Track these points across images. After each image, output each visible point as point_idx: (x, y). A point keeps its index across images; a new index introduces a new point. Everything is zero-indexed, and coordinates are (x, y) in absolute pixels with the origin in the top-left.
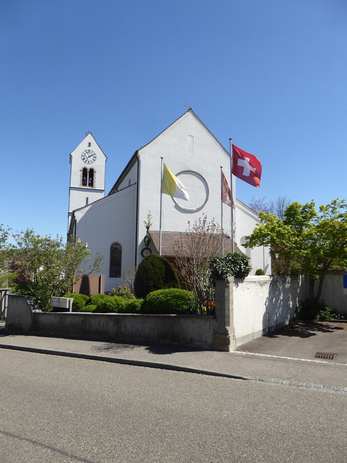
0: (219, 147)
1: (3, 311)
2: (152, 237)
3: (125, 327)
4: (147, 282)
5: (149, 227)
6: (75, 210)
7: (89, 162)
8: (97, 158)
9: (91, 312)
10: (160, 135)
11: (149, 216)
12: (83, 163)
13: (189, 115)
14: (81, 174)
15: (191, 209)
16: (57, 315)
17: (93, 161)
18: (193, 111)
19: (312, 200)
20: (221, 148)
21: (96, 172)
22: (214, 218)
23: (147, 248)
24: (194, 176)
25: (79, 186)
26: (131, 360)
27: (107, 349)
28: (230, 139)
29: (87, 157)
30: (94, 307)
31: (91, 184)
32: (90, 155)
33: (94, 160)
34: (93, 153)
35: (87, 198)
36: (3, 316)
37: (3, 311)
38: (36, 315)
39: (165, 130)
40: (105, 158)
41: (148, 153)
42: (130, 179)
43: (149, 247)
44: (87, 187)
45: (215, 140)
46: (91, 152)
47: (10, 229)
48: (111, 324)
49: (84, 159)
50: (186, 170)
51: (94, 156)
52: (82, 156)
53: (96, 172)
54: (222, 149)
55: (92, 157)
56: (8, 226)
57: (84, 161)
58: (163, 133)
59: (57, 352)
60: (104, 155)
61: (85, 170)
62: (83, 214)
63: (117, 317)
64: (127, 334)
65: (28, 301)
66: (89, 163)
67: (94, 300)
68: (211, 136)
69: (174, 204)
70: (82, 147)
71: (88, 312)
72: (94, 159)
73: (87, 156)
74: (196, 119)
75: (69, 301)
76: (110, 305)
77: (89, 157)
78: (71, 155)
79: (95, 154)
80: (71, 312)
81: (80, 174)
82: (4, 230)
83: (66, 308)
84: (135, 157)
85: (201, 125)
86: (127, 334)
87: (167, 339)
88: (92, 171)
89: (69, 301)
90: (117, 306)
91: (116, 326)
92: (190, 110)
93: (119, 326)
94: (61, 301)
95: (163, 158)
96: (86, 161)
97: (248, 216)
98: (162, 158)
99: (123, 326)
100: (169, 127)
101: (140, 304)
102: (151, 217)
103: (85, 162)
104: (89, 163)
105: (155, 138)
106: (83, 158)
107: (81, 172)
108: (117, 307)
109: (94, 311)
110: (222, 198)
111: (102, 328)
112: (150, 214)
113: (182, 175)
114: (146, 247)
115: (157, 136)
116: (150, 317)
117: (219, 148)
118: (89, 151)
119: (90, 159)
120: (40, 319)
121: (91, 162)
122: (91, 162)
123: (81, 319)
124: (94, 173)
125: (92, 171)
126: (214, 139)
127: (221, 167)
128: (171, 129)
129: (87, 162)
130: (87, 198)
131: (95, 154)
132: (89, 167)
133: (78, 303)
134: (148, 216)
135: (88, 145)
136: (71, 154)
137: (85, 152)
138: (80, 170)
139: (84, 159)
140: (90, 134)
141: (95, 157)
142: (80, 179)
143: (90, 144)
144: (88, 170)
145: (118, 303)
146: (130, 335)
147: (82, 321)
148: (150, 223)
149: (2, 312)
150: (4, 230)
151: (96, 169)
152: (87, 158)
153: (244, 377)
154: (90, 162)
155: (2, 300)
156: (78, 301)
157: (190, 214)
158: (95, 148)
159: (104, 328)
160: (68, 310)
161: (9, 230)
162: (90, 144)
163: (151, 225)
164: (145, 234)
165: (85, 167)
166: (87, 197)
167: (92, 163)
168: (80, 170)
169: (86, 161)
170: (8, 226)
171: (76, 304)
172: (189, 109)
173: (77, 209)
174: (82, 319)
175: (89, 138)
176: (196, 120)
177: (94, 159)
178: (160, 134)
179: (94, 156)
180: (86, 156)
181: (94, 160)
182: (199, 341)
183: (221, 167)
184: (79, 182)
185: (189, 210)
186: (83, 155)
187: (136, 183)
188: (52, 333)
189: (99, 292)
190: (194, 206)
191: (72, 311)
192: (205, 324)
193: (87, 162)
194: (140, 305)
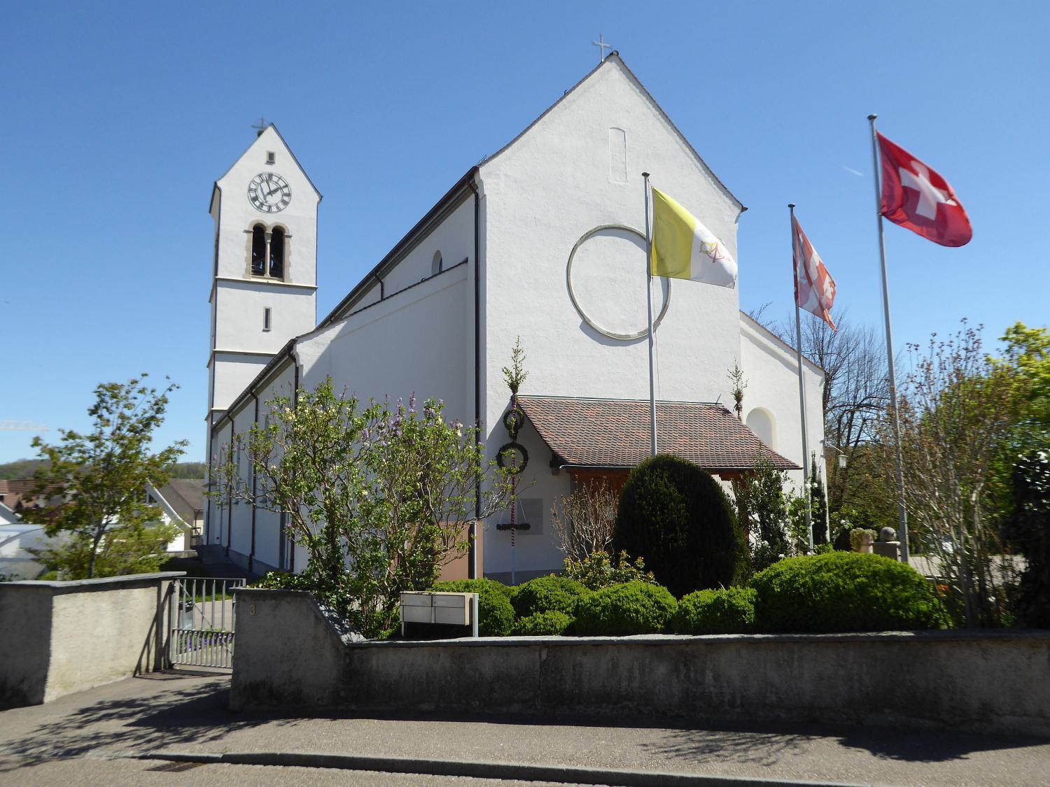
0: (692, 161)
1: (164, 642)
2: (528, 411)
3: (717, 678)
4: (670, 536)
5: (518, 384)
6: (297, 337)
7: (270, 207)
8: (293, 196)
9: (562, 635)
10: (537, 125)
11: (516, 352)
12: (251, 208)
13: (611, 71)
14: (248, 240)
15: (624, 334)
16: (440, 648)
17: (281, 206)
18: (621, 60)
19: (144, 375)
20: (699, 165)
21: (290, 237)
22: (935, 335)
23: (513, 445)
24: (627, 239)
25: (244, 277)
26: (278, 753)
27: (711, 749)
28: (871, 118)
29: (265, 193)
30: (564, 620)
31: (278, 271)
32: (273, 187)
33: (285, 203)
34: (282, 184)
35: (267, 311)
36: (164, 659)
37: (164, 642)
38: (356, 651)
39: (548, 111)
40: (317, 198)
41: (506, 175)
42: (438, 254)
43: (519, 441)
44: (267, 279)
45: (681, 142)
46: (275, 179)
47: (174, 388)
48: (661, 670)
49: (255, 199)
50: (607, 224)
51: (286, 190)
52: (250, 190)
53: (290, 237)
54: (701, 168)
55: (279, 194)
56: (168, 378)
57: (257, 203)
58: (545, 118)
59: (315, 757)
60: (313, 190)
61: (258, 231)
62: (322, 349)
63: (684, 646)
64: (726, 700)
65: (322, 608)
66: (269, 211)
67: (546, 597)
68: (672, 131)
69: (580, 321)
70: (250, 164)
71: (549, 633)
72: (286, 199)
73: (266, 190)
74: (630, 81)
75: (471, 601)
76: (637, 611)
77: (271, 193)
78: (216, 186)
79: (286, 186)
80: (476, 638)
81: (246, 240)
82: (153, 391)
83: (463, 627)
84: (466, 186)
85: (645, 98)
86: (726, 700)
87: (887, 711)
88: (279, 235)
89: (471, 601)
90: (658, 612)
91: (682, 676)
92: (612, 55)
93: (692, 674)
94: (439, 603)
95: (648, 175)
96: (262, 204)
97: (765, 354)
98: (646, 175)
99: (709, 676)
100: (558, 102)
101: (751, 603)
102: (520, 357)
103: (260, 207)
104: (269, 211)
105: (522, 134)
106: (253, 195)
107: (248, 237)
108: (661, 615)
109: (569, 631)
110: (796, 294)
111: (624, 684)
112: (519, 348)
113: (598, 238)
114: (510, 441)
115: (528, 128)
116: (812, 641)
117: (693, 165)
118: (271, 176)
119: (272, 200)
120: (374, 662)
121: (278, 208)
122: (278, 208)
123: (540, 657)
124: (287, 240)
125: (279, 235)
126: (678, 138)
127: (791, 206)
128: (565, 109)
129: (265, 208)
130: (267, 311)
131: (286, 186)
132: (270, 221)
133: (494, 608)
134: (513, 355)
135: (265, 158)
136: (220, 184)
137: (258, 180)
138: (247, 232)
139: (255, 199)
140: (270, 129)
141: (289, 195)
142: (245, 255)
143: (271, 158)
144: (270, 231)
145: (657, 602)
146: (739, 702)
147: (544, 664)
148: (522, 373)
149: (163, 645)
150: (153, 391)
151: (290, 228)
152: (265, 197)
153: (127, 760)
154: (274, 209)
155: (163, 611)
156: (495, 602)
157: (620, 348)
158: (286, 167)
159: (635, 684)
160: (467, 631)
161: (170, 390)
162: (271, 158)
163: (523, 377)
164: (505, 402)
165: (260, 222)
166: (268, 306)
167: (280, 210)
168: (247, 232)
169: (262, 204)
170: (168, 378)
171: (489, 611)
172: (612, 54)
173: (303, 336)
174: (544, 657)
175: (270, 140)
176: (631, 84)
177: (286, 199)
178: (535, 122)
179: (286, 190)
180: (262, 189)
181: (285, 203)
182: (1013, 713)
183: (791, 206)
184: (244, 265)
185: (620, 336)
186: (253, 186)
187: (466, 261)
188: (425, 707)
189: (471, 575)
190: (631, 326)
191: (480, 635)
192: (1029, 658)
193: (265, 208)
194: (752, 607)
